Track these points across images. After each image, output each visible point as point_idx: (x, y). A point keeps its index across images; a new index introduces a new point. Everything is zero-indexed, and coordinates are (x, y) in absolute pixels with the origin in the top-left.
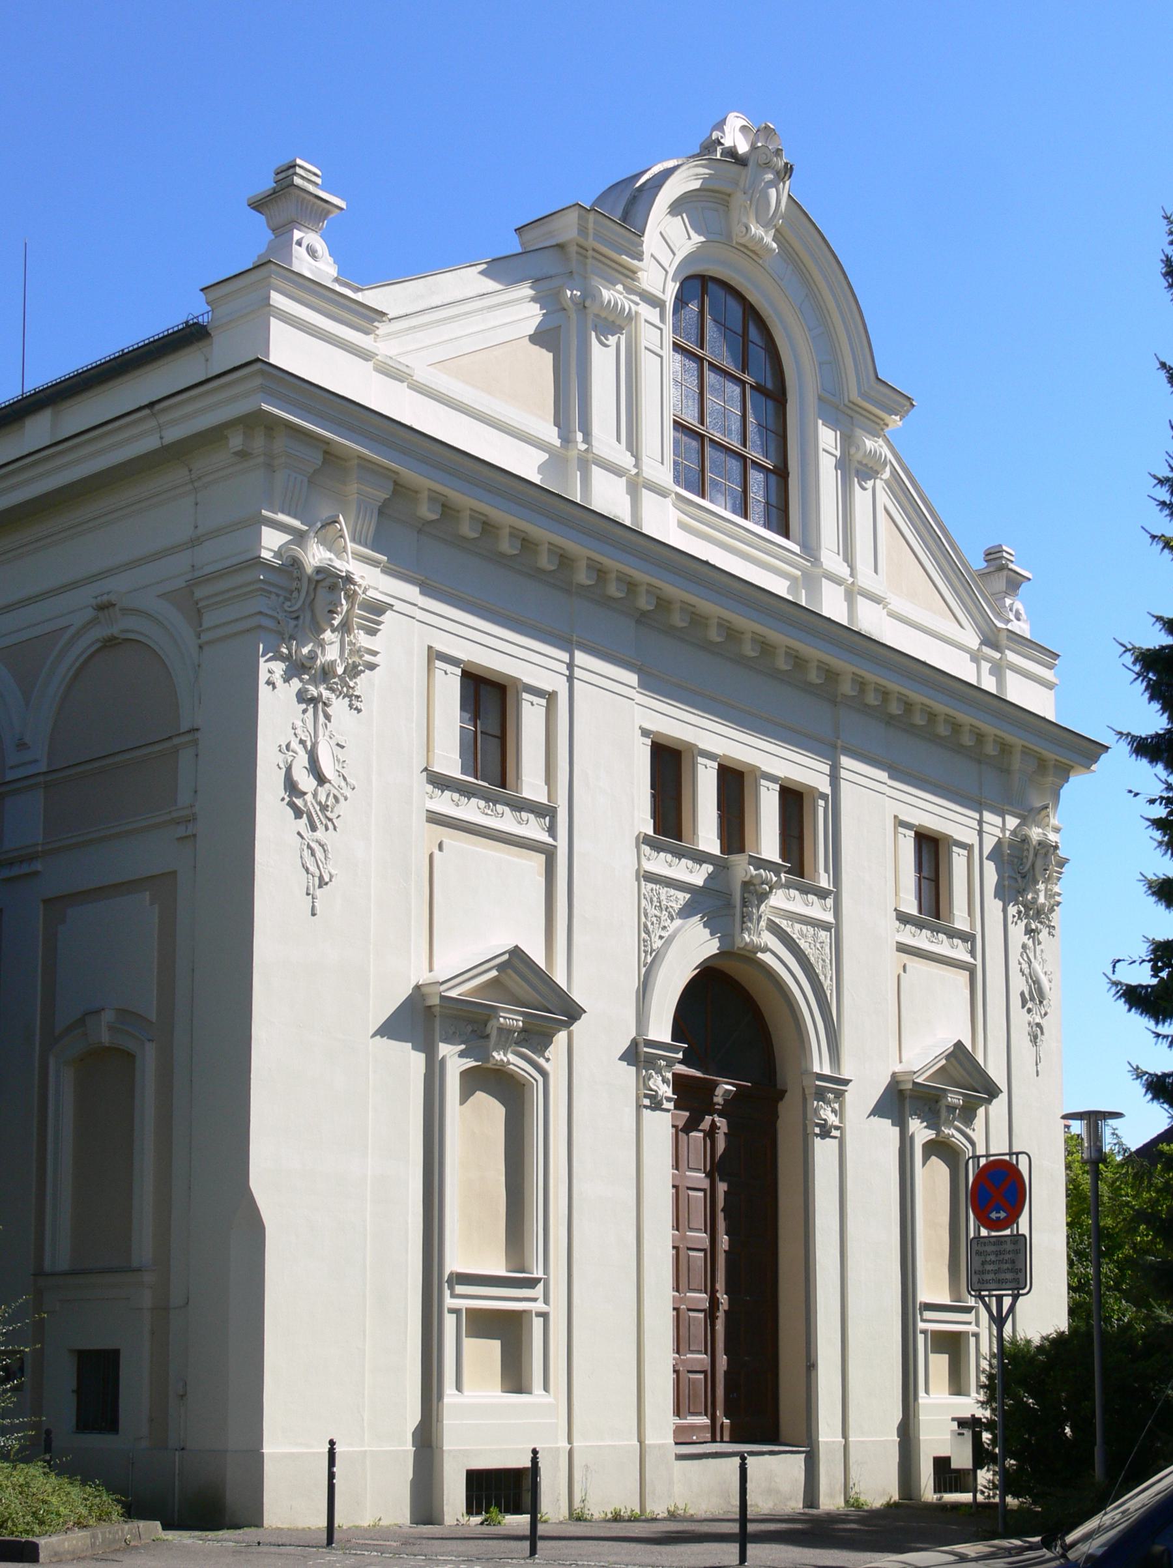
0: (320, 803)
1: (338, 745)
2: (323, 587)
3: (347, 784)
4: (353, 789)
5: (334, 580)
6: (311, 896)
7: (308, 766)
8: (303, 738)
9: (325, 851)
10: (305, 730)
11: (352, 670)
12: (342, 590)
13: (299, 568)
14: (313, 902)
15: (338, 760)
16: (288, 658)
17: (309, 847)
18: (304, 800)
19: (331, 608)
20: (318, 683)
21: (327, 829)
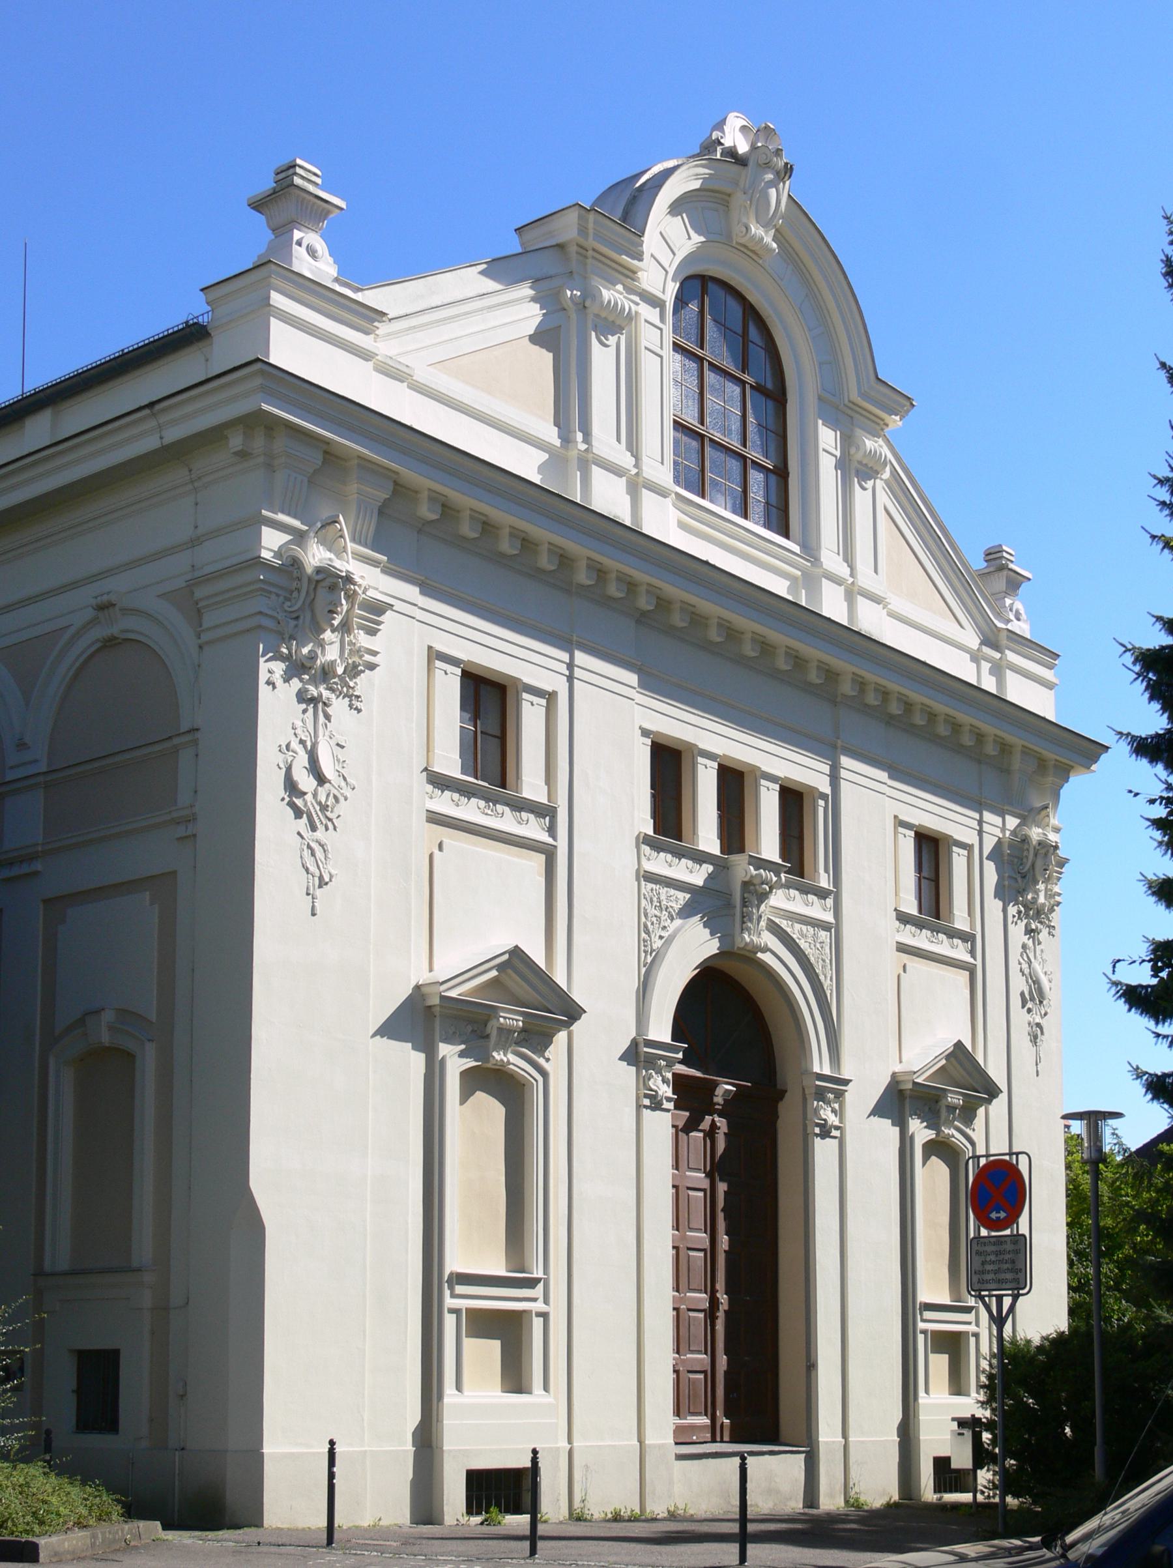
0: (320, 803)
1: (338, 745)
2: (323, 587)
3: (347, 784)
4: (353, 789)
5: (334, 580)
6: (311, 896)
7: (308, 766)
9: (325, 851)
10: (305, 730)
11: (352, 670)
12: (342, 590)
13: (299, 568)
14: (313, 902)
16: (288, 658)
17: (309, 847)
18: (304, 800)
19: (331, 608)
20: (318, 683)
21: (327, 829)
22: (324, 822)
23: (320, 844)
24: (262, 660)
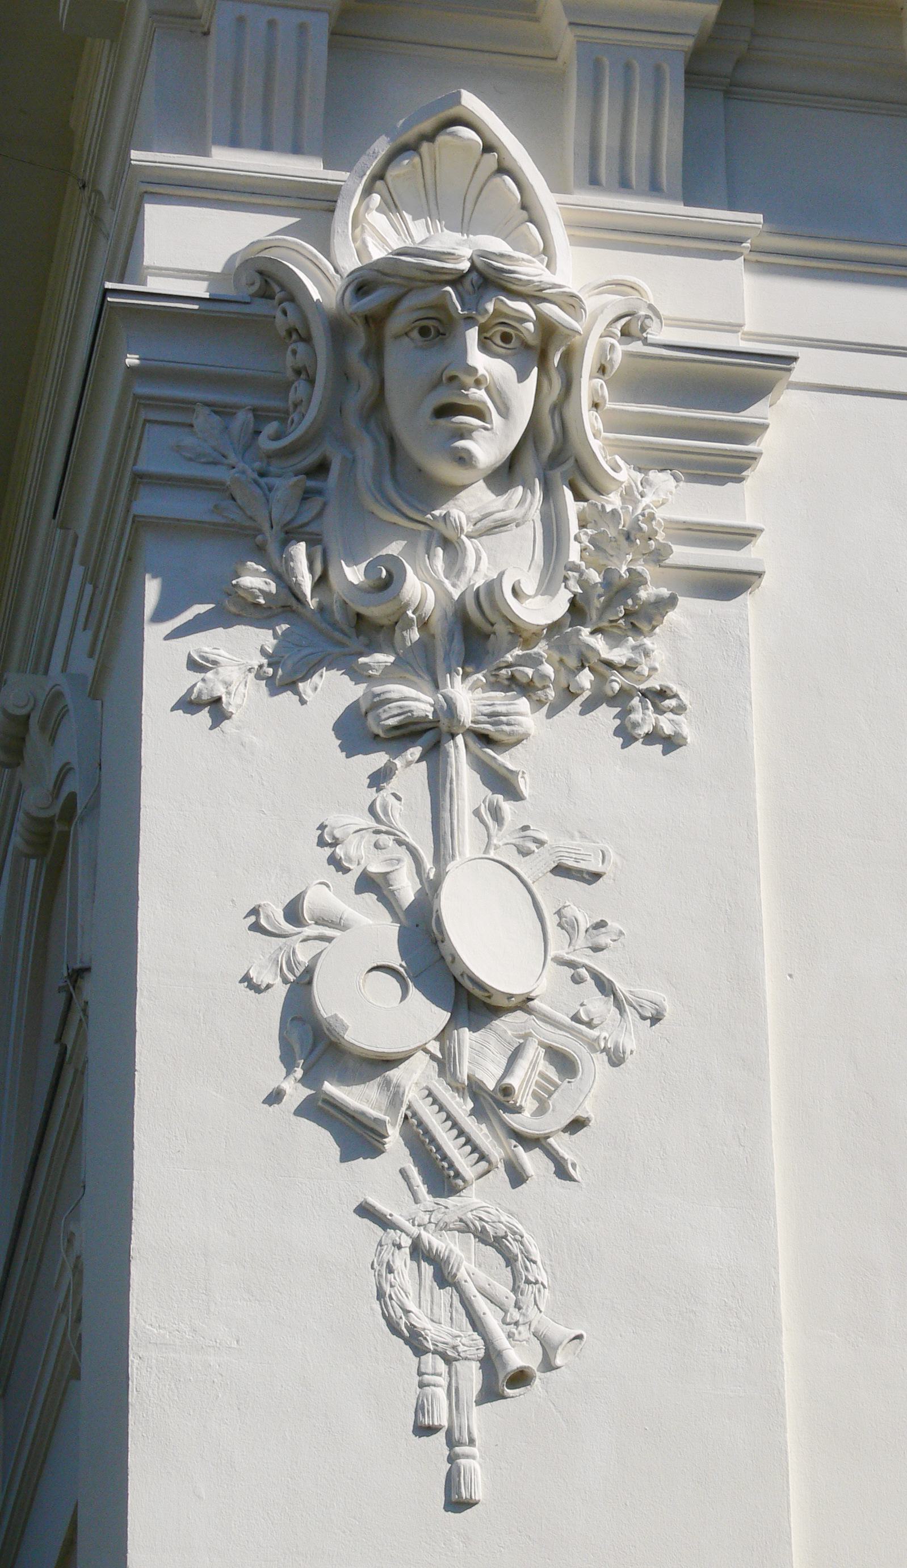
0: (474, 1089)
1: (561, 870)
2: (397, 337)
3: (618, 1004)
4: (655, 1020)
5: (431, 296)
6: (441, 1437)
7: (396, 960)
8: (374, 868)
9: (510, 1261)
10: (387, 840)
11: (608, 605)
12: (470, 320)
13: (292, 299)
14: (452, 1459)
15: (568, 926)
16: (286, 608)
17: (419, 1251)
18: (388, 1083)
19: (445, 396)
20: (440, 666)
21: (517, 1177)
22: (496, 1153)
23: (482, 1237)
24: (154, 635)
